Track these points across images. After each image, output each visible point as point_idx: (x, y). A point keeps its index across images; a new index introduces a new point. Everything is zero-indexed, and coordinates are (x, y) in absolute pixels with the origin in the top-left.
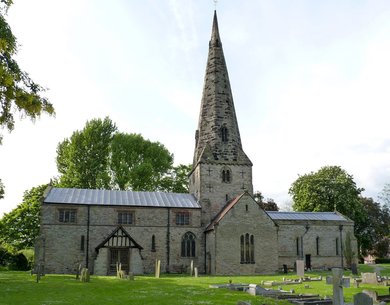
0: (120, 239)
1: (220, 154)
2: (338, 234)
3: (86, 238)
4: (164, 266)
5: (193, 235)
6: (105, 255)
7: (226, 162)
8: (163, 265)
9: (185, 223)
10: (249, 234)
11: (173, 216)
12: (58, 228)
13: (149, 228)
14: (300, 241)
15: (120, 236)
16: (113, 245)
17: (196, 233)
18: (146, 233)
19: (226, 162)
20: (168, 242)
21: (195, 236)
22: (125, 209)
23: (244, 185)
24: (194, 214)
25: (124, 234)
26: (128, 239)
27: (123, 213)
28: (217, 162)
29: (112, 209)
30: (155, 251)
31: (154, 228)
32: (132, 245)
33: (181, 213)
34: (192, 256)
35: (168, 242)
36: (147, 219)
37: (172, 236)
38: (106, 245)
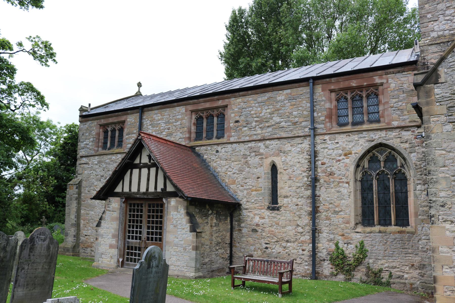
4: (304, 252)
5: (396, 155)
8: (300, 251)
9: (365, 118)
12: (96, 162)
13: (261, 144)
15: (145, 166)
16: (130, 190)
18: (254, 160)
20: (314, 182)
21: (404, 159)
22: (208, 105)
24: (393, 85)
27: (204, 115)
29: (181, 111)
30: (278, 209)
31: (272, 142)
33: (352, 89)
34: (396, 225)
35: (314, 182)
36: (256, 121)
37: (325, 160)
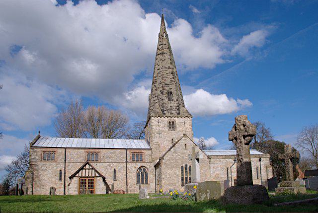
0: (87, 171)
1: (167, 110)
2: (258, 164)
3: (63, 172)
6: (76, 182)
7: (171, 116)
10: (187, 164)
11: (130, 155)
14: (229, 171)
17: (148, 167)
18: (108, 167)
19: (171, 116)
23: (185, 131)
25: (91, 167)
26: (93, 171)
28: (165, 116)
29: (83, 151)
32: (97, 175)
38: (77, 175)
